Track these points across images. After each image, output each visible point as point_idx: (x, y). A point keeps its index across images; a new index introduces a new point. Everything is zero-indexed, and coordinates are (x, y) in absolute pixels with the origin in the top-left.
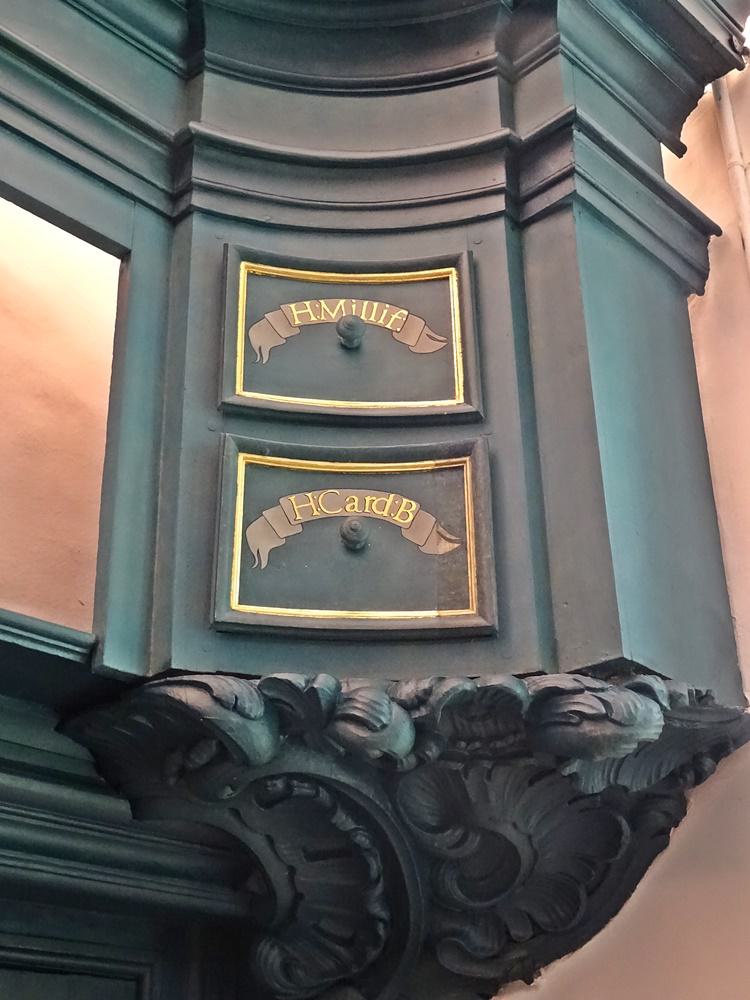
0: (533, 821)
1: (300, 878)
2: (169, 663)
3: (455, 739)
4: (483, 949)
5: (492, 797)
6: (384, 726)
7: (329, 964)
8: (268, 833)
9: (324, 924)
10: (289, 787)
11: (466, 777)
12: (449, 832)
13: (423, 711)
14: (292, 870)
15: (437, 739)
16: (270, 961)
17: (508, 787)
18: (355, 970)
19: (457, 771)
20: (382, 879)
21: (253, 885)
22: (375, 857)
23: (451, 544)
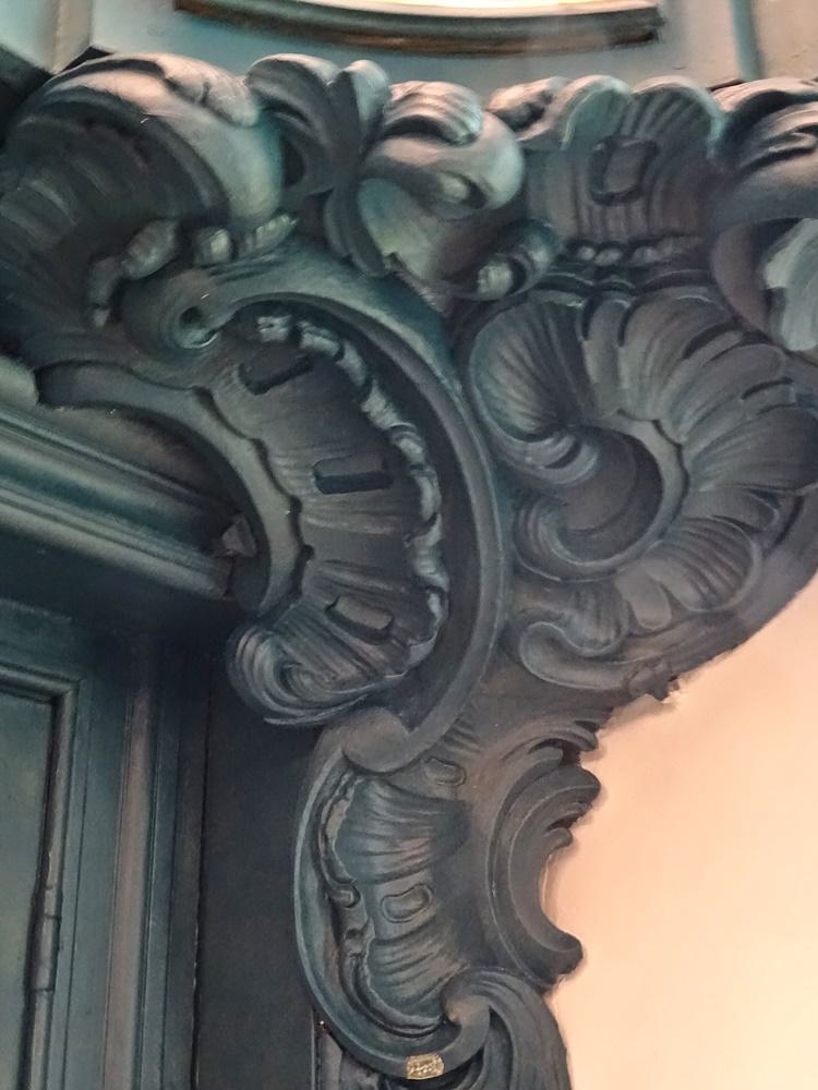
0: (688, 423)
1: (307, 519)
2: (88, 40)
3: (575, 244)
4: (593, 643)
5: (625, 370)
6: (472, 138)
7: (348, 670)
8: (256, 437)
9: (343, 607)
10: (295, 335)
11: (586, 336)
12: (548, 442)
13: (538, 129)
14: (296, 505)
15: (548, 236)
16: (257, 662)
17: (651, 359)
18: (391, 677)
19: (572, 309)
20: (439, 520)
21: (232, 541)
22: (429, 477)
23: (382, 895)
